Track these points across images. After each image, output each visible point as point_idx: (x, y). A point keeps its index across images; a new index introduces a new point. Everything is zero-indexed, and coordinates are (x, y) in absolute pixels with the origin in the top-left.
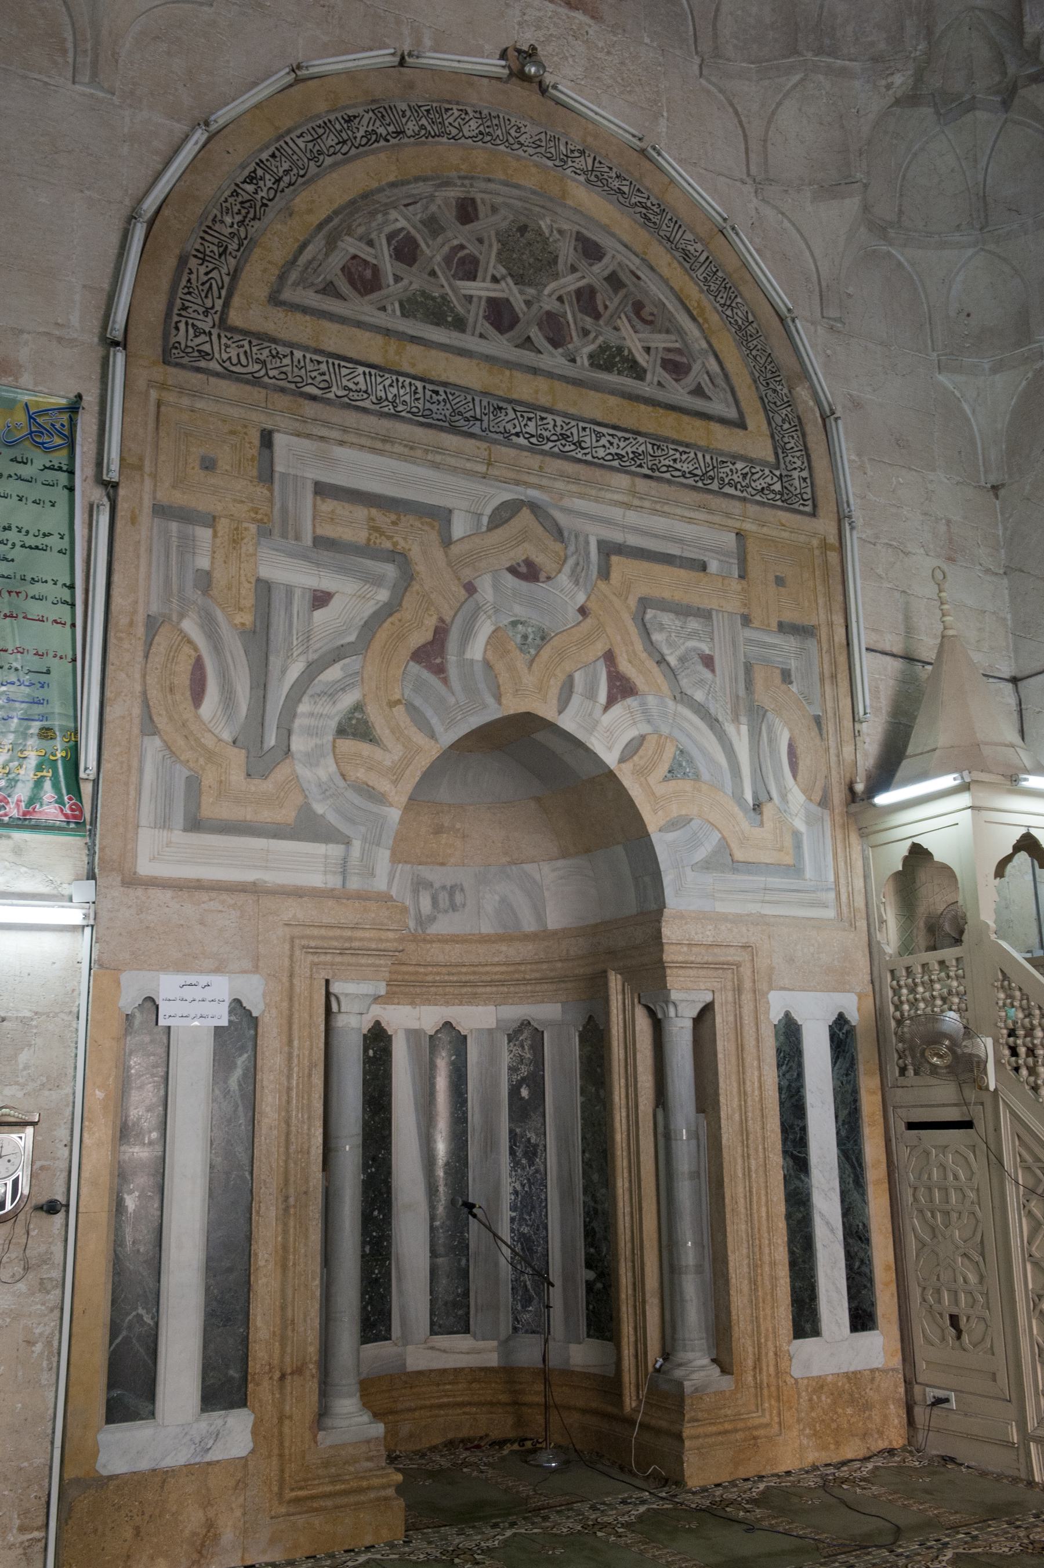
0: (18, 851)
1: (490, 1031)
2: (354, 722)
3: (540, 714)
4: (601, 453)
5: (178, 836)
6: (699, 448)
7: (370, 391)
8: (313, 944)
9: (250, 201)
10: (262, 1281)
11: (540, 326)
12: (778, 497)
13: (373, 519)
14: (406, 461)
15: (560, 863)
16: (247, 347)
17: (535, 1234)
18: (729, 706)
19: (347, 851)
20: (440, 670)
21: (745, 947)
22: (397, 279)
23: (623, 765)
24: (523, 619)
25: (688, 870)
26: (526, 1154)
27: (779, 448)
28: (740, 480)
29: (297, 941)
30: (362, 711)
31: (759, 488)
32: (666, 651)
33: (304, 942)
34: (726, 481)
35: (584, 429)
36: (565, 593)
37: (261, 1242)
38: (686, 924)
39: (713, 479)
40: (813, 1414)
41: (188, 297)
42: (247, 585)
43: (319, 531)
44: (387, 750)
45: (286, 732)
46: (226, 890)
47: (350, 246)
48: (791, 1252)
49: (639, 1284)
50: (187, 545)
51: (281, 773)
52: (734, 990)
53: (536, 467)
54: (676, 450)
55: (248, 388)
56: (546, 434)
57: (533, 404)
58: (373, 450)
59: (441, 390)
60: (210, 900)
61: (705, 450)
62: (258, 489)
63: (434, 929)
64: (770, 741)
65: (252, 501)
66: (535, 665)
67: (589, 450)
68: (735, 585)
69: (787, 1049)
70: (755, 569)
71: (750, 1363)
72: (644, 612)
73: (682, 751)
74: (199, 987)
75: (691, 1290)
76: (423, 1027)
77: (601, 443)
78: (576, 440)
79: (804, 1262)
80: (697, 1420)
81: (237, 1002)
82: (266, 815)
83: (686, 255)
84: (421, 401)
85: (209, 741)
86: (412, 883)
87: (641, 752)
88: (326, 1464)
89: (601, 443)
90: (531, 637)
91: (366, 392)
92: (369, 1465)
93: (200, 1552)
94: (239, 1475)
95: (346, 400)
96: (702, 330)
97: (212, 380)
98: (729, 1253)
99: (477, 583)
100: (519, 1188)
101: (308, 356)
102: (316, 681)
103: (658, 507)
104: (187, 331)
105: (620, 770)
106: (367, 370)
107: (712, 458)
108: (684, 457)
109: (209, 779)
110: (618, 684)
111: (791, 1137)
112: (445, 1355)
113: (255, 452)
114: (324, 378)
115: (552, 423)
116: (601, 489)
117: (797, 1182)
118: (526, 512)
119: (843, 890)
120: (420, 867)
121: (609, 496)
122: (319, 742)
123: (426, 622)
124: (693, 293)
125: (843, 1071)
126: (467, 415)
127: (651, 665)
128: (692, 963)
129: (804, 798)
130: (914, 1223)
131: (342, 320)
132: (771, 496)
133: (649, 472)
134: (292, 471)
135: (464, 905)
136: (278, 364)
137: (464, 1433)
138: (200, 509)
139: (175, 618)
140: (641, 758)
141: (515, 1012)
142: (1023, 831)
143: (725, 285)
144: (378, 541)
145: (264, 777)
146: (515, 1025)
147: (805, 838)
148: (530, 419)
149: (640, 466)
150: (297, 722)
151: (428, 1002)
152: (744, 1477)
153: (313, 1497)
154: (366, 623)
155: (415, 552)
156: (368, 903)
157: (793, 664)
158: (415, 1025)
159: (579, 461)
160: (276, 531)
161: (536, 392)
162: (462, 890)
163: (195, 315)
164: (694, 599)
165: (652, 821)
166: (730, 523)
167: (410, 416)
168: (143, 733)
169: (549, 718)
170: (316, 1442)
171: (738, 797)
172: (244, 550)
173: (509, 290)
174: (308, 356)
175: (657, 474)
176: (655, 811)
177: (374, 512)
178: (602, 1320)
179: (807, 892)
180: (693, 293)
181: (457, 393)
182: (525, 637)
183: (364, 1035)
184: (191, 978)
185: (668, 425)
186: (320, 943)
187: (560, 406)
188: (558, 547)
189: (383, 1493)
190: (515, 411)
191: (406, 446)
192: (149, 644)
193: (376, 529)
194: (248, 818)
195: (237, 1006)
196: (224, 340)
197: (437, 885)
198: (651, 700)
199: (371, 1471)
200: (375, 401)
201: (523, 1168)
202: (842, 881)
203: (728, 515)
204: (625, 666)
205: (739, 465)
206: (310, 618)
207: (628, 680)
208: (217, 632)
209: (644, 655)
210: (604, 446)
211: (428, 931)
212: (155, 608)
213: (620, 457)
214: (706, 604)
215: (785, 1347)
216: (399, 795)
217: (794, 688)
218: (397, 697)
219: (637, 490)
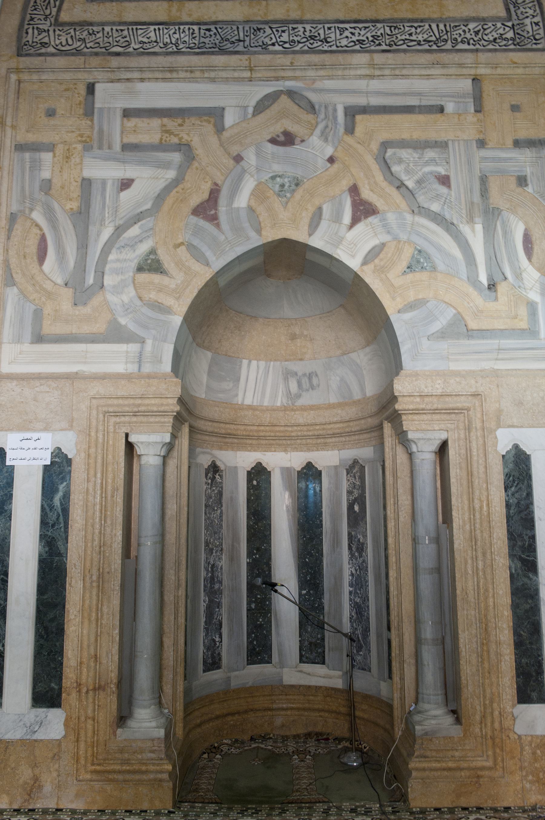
1: (336, 467)
2: (149, 261)
3: (294, 238)
4: (344, 42)
5: (27, 347)
6: (433, 20)
7: (158, 40)
8: (111, 409)
10: (72, 628)
12: (510, 42)
13: (165, 126)
14: (190, 82)
15: (368, 349)
16: (73, 33)
17: (363, 603)
18: (464, 211)
19: (142, 348)
20: (214, 219)
21: (475, 395)
23: (365, 268)
24: (280, 174)
25: (424, 341)
26: (357, 549)
28: (473, 36)
29: (100, 408)
30: (156, 254)
31: (492, 39)
32: (404, 177)
33: (105, 409)
34: (459, 40)
35: (329, 28)
36: (317, 147)
37: (71, 603)
38: (416, 380)
39: (446, 41)
40: (537, 765)
41: (35, 12)
42: (75, 184)
43: (126, 140)
44: (173, 278)
45: (100, 274)
46: (51, 378)
48: (516, 633)
50: (36, 166)
51: (96, 301)
52: (465, 429)
53: (289, 64)
54: (412, 26)
55: (73, 58)
56: (296, 39)
57: (286, 20)
58: (164, 79)
59: (212, 27)
60: (41, 385)
61: (438, 21)
62: (83, 122)
65: (79, 130)
66: (290, 204)
67: (334, 42)
68: (471, 118)
69: (517, 474)
70: (489, 102)
71: (478, 717)
72: (386, 152)
73: (420, 251)
74: (32, 441)
76: (293, 465)
77: (344, 35)
78: (322, 37)
79: (531, 643)
80: (425, 757)
82: (86, 329)
84: (197, 39)
85: (48, 286)
86: (283, 374)
87: (381, 256)
88: (121, 751)
89: (344, 35)
90: (287, 185)
91: (156, 42)
92: (153, 755)
93: (29, 795)
94: (56, 751)
95: (142, 50)
97: (48, 58)
98: (460, 632)
99: (243, 154)
100: (354, 572)
101: (114, 28)
102: (121, 238)
103: (397, 72)
104: (33, 33)
105: (363, 271)
106: (157, 27)
107: (445, 26)
108: (419, 30)
109: (48, 310)
110: (362, 208)
112: (309, 677)
113: (81, 99)
114: (126, 39)
115: (302, 30)
116: (344, 69)
118: (284, 99)
120: (287, 363)
121: (352, 72)
122: (123, 278)
123: (203, 187)
126: (233, 40)
128: (423, 410)
129: (539, 275)
132: (504, 42)
133: (388, 48)
134: (106, 106)
135: (319, 386)
136: (94, 38)
137: (319, 729)
138: (44, 141)
139: (27, 212)
140: (381, 260)
141: (350, 454)
144: (168, 139)
146: (350, 462)
147: (540, 307)
148: (283, 31)
149: (380, 44)
150: (108, 267)
151: (296, 449)
152: (465, 805)
153: (109, 772)
154: (159, 195)
155: (196, 142)
156: (151, 381)
157: (528, 171)
158: (288, 465)
159: (326, 52)
160: (95, 145)
161: (288, 11)
162: (317, 375)
163: (39, 22)
164: (432, 135)
165: (391, 306)
166: (465, 71)
167: (189, 50)
168: (6, 285)
169: (301, 240)
170: (115, 735)
171: (474, 281)
172: (73, 160)
174: (114, 28)
175: (395, 47)
176: (394, 298)
177: (165, 120)
181: (225, 27)
182: (282, 186)
183: (248, 472)
184: (28, 435)
186: (116, 409)
187: (308, 17)
188: (310, 117)
189: (159, 776)
190: (271, 28)
191: (186, 71)
192: (10, 230)
193: (167, 132)
194: (74, 332)
195: (58, 453)
196: (57, 32)
197: (300, 374)
198: (391, 217)
199: (152, 759)
200: (162, 46)
201: (356, 559)
203: (461, 65)
204: (366, 194)
205: (472, 26)
206: (118, 199)
207: (370, 204)
208: (55, 216)
209: (384, 184)
210: (347, 37)
211: (296, 404)
212: (14, 208)
213: (360, 42)
214: (443, 137)
215: (509, 709)
217: (530, 189)
218: (180, 241)
219: (375, 62)
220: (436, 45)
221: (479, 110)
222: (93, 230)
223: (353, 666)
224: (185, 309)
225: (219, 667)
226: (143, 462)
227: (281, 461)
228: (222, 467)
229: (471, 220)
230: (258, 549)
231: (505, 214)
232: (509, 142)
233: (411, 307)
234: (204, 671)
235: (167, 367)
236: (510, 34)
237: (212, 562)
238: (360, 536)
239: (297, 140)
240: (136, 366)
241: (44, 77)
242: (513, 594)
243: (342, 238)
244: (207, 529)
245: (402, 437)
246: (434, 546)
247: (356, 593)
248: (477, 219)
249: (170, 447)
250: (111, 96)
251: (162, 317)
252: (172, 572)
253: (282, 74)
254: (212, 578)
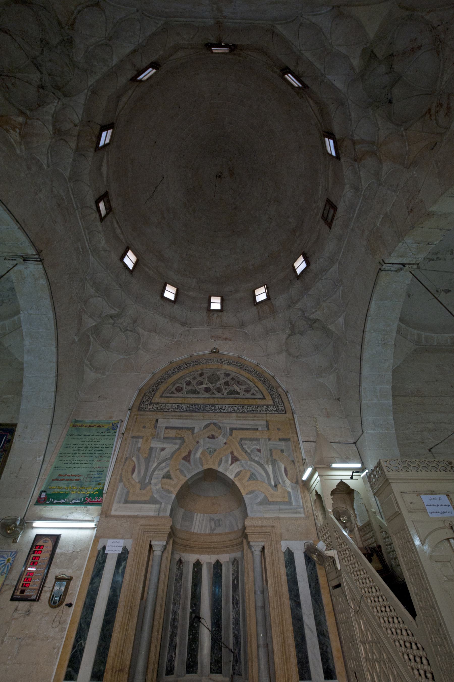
0: (87, 510)
1: (228, 562)
4: (230, 410)
5: (122, 505)
8: (146, 530)
11: (216, 390)
20: (189, 461)
22: (186, 388)
25: (255, 505)
26: (236, 603)
32: (247, 449)
33: (144, 530)
36: (221, 440)
43: (165, 436)
45: (151, 479)
47: (177, 385)
48: (296, 640)
50: (137, 443)
58: (178, 419)
63: (215, 532)
64: (278, 468)
79: (302, 645)
81: (125, 547)
82: (143, 499)
83: (249, 371)
87: (241, 475)
96: (253, 383)
111: (293, 593)
117: (297, 611)
118: (212, 425)
119: (305, 508)
125: (311, 569)
127: (243, 453)
131: (174, 397)
142: (340, 481)
145: (144, 489)
146: (233, 559)
151: (213, 553)
155: (186, 437)
157: (284, 448)
158: (209, 561)
165: (243, 492)
177: (177, 430)
179: (294, 509)
180: (251, 377)
182: (210, 451)
184: (115, 540)
185: (246, 402)
187: (220, 403)
188: (220, 431)
192: (125, 463)
195: (125, 549)
197: (215, 520)
202: (305, 505)
203: (262, 417)
204: (236, 454)
205: (264, 407)
209: (241, 451)
212: (127, 456)
213: (234, 410)
217: (285, 454)
218: (178, 468)
220: (255, 412)
221: (268, 429)
222: (151, 464)
223: (234, 673)
224: (176, 492)
225: (173, 674)
226: (154, 554)
227: (207, 559)
228: (183, 561)
229: (268, 463)
230: (195, 604)
231: (278, 461)
232: (278, 439)
233: (250, 493)
234: (166, 675)
235: (168, 514)
236: (275, 409)
237: (175, 610)
238: (237, 597)
239: (216, 437)
240: (158, 513)
241: (144, 417)
242: (292, 619)
243: (228, 468)
244: (175, 592)
245: (250, 547)
246: (262, 595)
247: (235, 628)
248: (270, 463)
249: (165, 547)
250: (162, 423)
251: (169, 495)
252: (159, 609)
253: (212, 418)
254: (174, 619)
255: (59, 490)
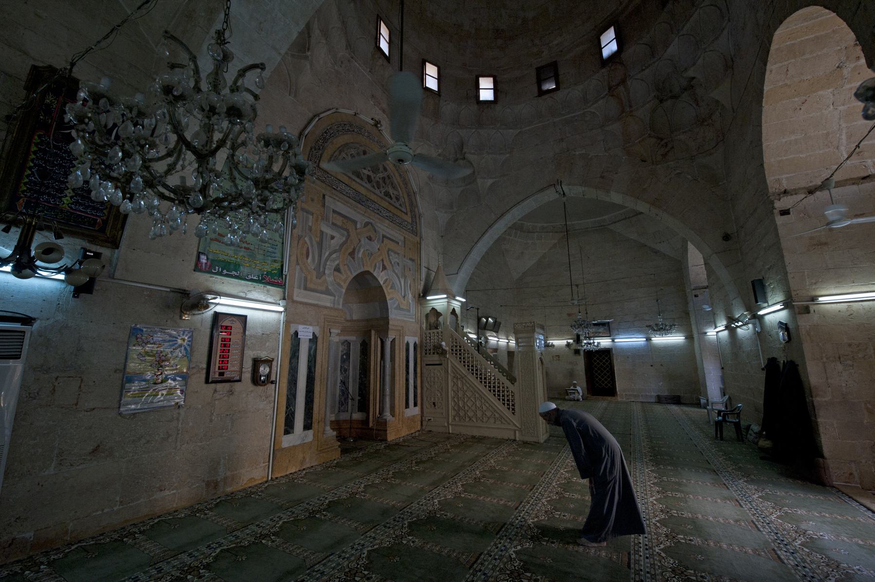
9: (326, 137)
20: (353, 258)
27: (412, 221)
49: (375, 399)
51: (323, 278)
75: (388, 399)
124: (401, 183)
130: (426, 384)
143: (406, 183)
165: (388, 298)
173: (370, 173)
178: (363, 406)
216: (345, 286)
255: (225, 257)
